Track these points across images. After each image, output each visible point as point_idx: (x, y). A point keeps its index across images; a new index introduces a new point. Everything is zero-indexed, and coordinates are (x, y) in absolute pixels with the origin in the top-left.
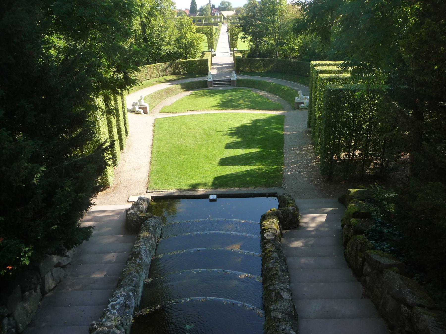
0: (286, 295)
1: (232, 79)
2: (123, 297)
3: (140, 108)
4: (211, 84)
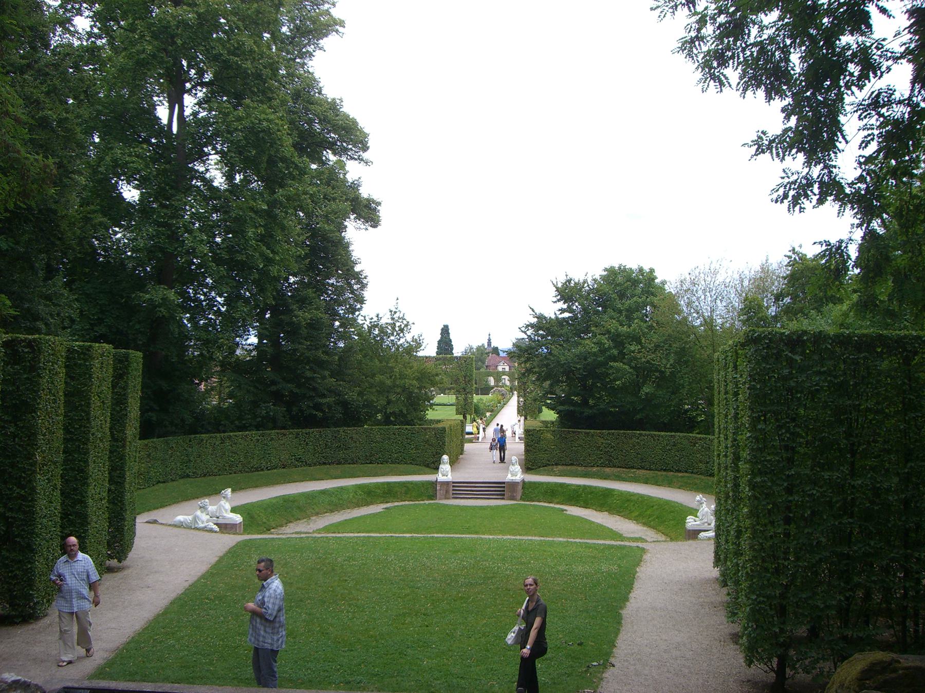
1: (509, 478)
4: (447, 492)
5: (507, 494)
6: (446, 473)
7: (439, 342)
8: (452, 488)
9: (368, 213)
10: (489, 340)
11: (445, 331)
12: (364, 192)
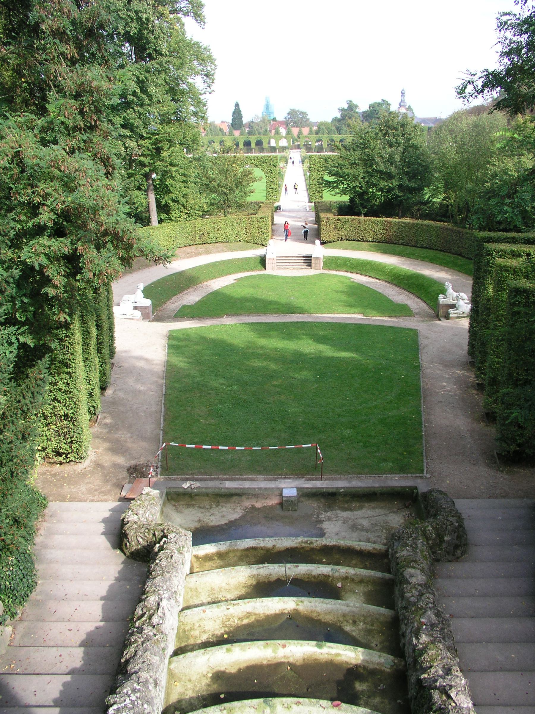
7: (234, 113)
8: (276, 261)
11: (237, 105)
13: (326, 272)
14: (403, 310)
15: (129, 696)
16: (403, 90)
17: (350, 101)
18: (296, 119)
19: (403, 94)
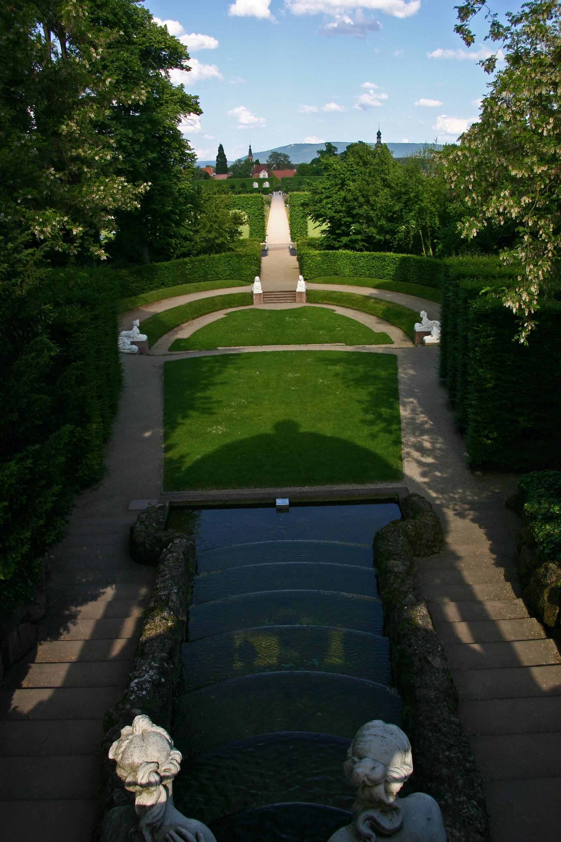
0: (437, 662)
2: (154, 671)
3: (133, 343)
5: (298, 299)
6: (257, 287)
7: (218, 157)
9: (190, 105)
10: (250, 150)
11: (221, 149)
12: (187, 91)
13: (309, 305)
14: (384, 338)
15: (148, 672)
16: (379, 132)
17: (329, 143)
18: (278, 160)
19: (379, 134)
